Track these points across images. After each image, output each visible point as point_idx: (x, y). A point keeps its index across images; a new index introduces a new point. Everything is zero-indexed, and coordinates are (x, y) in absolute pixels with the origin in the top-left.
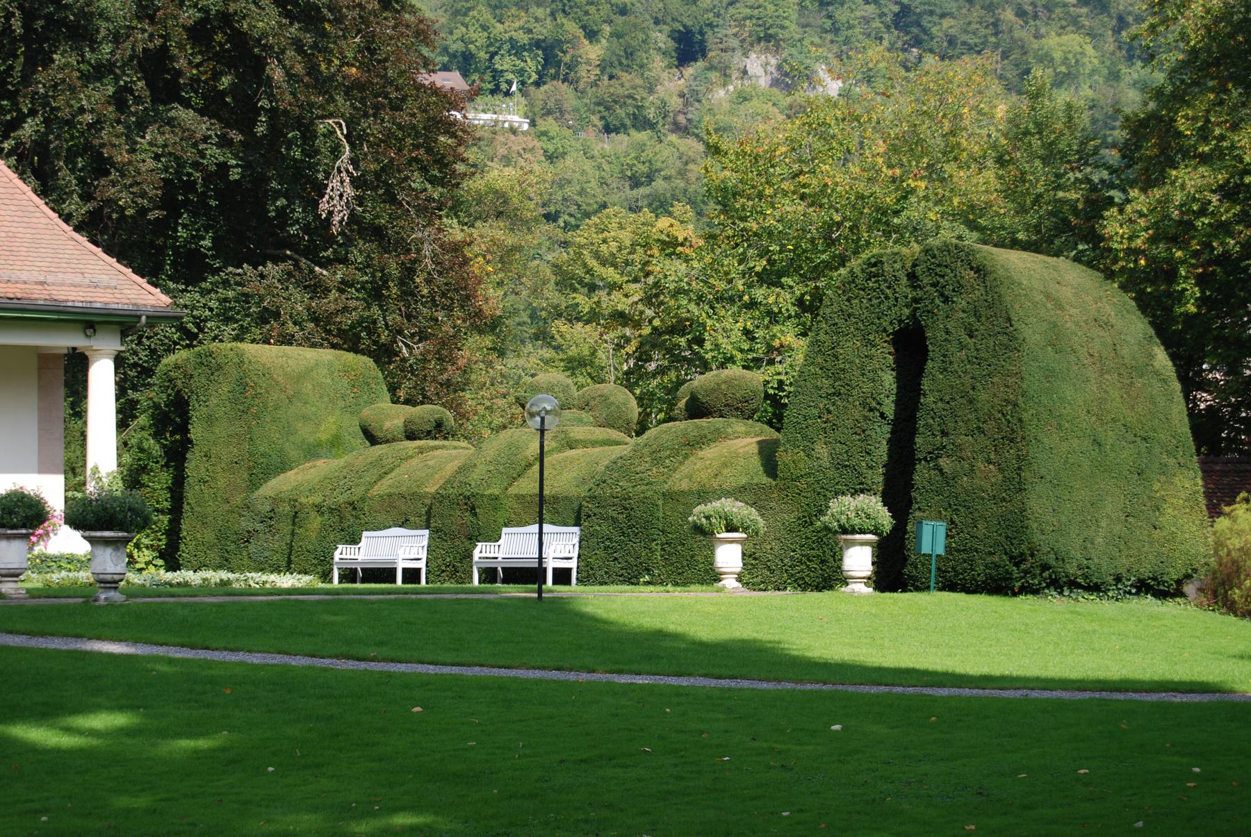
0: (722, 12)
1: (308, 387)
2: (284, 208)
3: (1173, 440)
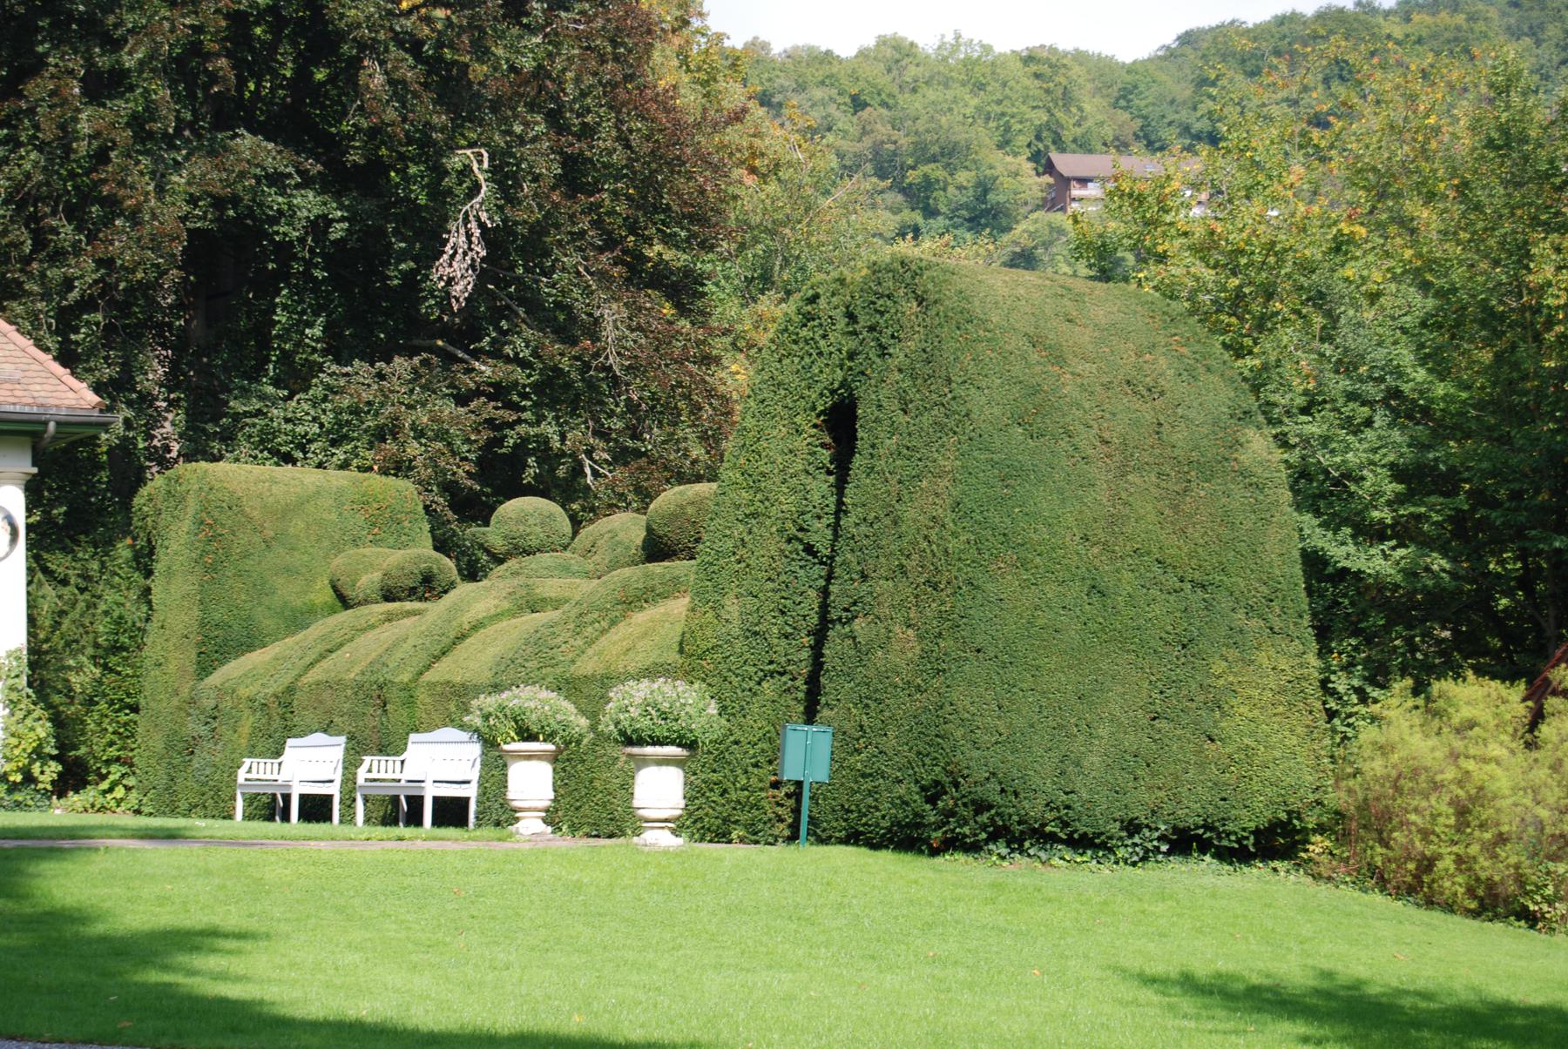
0: (1553, 72)
1: (297, 525)
2: (413, 272)
3: (1264, 589)
